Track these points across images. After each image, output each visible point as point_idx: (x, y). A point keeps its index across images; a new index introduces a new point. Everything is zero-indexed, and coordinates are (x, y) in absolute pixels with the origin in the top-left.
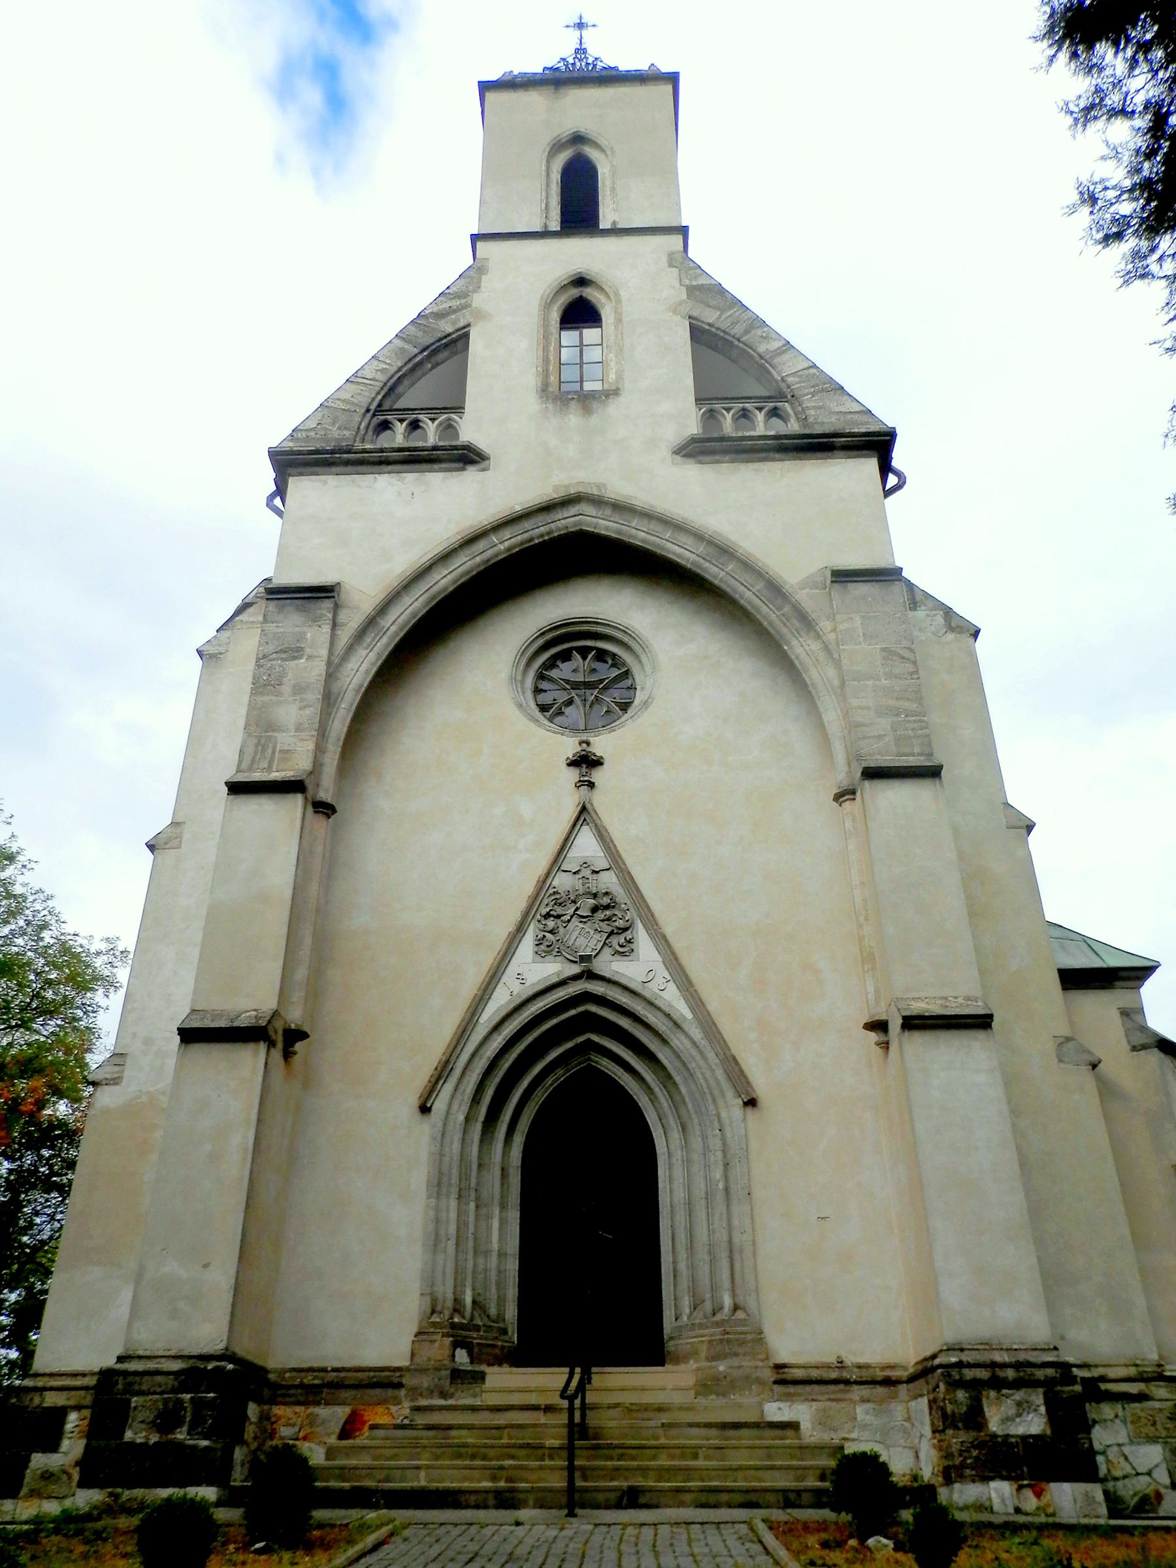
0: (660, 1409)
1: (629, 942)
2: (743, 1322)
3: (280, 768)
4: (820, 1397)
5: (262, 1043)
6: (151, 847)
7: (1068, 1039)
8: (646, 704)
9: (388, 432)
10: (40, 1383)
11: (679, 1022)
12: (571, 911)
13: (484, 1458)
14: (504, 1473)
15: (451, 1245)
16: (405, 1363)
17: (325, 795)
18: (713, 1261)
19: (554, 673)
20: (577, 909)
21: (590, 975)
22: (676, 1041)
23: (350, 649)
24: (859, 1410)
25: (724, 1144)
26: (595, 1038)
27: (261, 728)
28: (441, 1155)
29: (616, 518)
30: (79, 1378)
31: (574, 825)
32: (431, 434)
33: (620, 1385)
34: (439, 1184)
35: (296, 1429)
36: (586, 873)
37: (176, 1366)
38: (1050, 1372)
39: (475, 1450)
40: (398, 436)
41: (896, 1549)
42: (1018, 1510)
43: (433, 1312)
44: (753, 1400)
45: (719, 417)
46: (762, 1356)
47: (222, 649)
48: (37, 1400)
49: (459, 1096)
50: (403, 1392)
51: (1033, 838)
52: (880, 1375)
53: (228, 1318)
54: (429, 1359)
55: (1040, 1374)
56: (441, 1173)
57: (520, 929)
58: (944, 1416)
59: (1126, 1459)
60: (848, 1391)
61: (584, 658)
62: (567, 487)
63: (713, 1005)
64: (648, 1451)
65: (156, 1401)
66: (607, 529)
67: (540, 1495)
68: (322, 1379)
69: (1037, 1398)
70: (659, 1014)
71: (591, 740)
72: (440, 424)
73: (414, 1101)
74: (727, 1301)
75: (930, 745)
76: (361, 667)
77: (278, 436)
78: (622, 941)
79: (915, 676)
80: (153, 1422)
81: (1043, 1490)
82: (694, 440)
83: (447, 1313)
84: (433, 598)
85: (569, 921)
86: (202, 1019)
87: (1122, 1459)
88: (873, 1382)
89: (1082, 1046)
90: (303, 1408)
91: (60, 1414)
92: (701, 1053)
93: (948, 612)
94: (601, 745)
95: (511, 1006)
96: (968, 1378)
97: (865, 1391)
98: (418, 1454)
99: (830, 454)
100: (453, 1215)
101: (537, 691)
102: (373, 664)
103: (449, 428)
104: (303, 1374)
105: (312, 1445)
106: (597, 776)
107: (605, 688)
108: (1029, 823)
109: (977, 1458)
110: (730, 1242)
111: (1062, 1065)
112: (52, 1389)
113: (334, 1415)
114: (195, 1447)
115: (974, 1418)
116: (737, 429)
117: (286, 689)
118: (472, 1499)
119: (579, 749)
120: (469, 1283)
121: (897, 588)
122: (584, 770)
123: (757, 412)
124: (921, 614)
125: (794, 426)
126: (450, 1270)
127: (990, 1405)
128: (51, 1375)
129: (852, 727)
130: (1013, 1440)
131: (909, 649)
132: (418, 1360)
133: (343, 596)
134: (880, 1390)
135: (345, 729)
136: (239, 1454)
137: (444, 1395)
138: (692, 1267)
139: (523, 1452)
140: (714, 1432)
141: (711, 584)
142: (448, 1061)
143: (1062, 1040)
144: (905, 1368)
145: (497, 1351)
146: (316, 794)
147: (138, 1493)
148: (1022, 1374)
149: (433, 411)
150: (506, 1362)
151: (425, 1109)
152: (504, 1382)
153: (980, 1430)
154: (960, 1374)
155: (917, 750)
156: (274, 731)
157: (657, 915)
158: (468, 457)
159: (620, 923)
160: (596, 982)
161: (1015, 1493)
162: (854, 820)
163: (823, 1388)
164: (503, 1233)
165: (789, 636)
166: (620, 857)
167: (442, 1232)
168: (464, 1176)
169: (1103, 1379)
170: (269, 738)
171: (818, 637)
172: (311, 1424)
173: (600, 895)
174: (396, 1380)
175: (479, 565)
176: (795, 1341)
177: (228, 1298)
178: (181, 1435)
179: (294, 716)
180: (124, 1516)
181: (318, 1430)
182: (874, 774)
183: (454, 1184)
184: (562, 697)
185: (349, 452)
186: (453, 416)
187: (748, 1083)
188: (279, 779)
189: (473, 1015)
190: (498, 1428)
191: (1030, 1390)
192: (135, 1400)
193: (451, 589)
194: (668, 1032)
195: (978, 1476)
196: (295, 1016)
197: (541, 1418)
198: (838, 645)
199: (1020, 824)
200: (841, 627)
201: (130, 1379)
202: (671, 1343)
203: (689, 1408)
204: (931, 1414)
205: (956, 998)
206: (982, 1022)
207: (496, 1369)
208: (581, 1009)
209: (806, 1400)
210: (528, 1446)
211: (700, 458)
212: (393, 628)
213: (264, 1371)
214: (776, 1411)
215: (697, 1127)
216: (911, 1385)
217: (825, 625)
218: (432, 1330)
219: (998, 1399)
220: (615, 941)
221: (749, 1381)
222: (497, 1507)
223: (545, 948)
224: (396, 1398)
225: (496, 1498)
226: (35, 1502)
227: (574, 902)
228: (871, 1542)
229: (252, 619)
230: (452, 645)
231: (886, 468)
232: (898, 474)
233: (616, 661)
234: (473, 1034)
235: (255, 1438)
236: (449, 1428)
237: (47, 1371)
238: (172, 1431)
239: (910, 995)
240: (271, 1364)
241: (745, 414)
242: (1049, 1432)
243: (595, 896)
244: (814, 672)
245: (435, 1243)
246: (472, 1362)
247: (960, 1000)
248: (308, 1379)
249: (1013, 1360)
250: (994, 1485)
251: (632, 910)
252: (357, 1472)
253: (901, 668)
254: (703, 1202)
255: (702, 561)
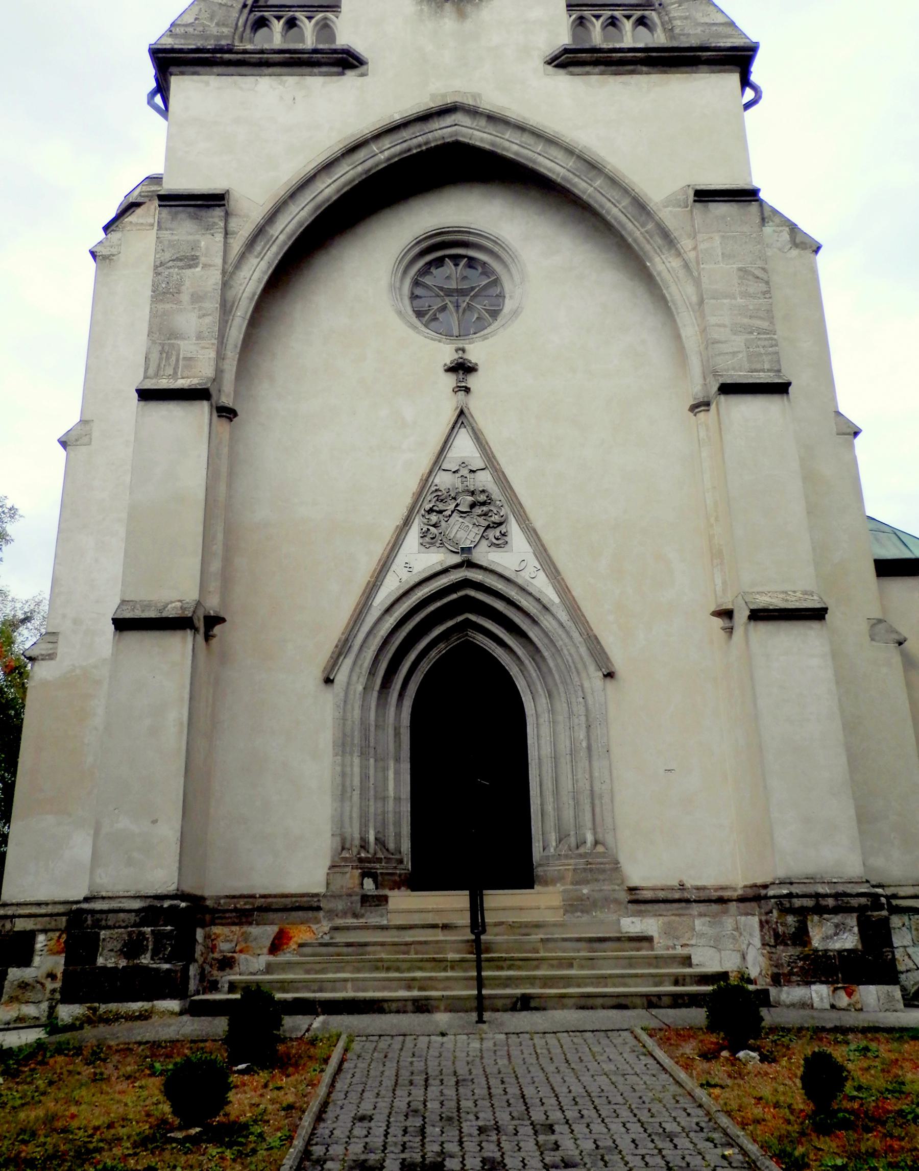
0: (538, 926)
1: (504, 535)
2: (603, 855)
3: (185, 375)
4: (665, 913)
5: (189, 631)
6: (64, 444)
7: (880, 621)
8: (516, 313)
9: (265, 29)
10: (10, 911)
11: (548, 606)
12: (452, 507)
13: (398, 970)
14: (416, 984)
15: (356, 796)
16: (321, 889)
17: (226, 400)
18: (577, 804)
19: (428, 280)
20: (457, 505)
21: (470, 564)
22: (545, 622)
23: (242, 257)
24: (697, 922)
25: (587, 710)
26: (473, 618)
27: (163, 337)
28: (344, 719)
29: (491, 129)
30: (43, 906)
31: (453, 428)
32: (309, 36)
33: (501, 903)
34: (343, 745)
35: (233, 944)
36: (464, 472)
37: (137, 905)
38: (863, 900)
39: (389, 964)
40: (275, 37)
41: (762, 1061)
42: (833, 1006)
43: (343, 849)
44: (614, 917)
45: (588, 24)
46: (619, 882)
47: (114, 251)
48: (8, 926)
49: (357, 669)
50: (321, 914)
51: (858, 441)
52: (715, 895)
53: (177, 865)
54: (342, 887)
55: (855, 902)
56: (344, 735)
57: (407, 523)
58: (776, 935)
59: (910, 957)
60: (688, 908)
61: (456, 265)
62: (444, 96)
63: (578, 592)
64: (531, 962)
65: (121, 934)
66: (482, 140)
67: (449, 1002)
68: (253, 904)
69: (852, 921)
70: (531, 599)
71: (467, 347)
72: (317, 23)
73: (316, 673)
74: (590, 838)
75: (778, 361)
76: (254, 274)
77: (154, 30)
78: (498, 534)
79: (767, 296)
80: (121, 950)
81: (854, 991)
82: (566, 51)
83: (355, 850)
84: (319, 207)
85: (450, 516)
86: (133, 610)
87: (906, 957)
88: (709, 901)
89: (891, 626)
90: (238, 928)
91: (30, 936)
92: (567, 633)
93: (793, 228)
94: (475, 352)
95: (401, 591)
96: (796, 906)
97: (702, 907)
98: (343, 967)
99: (694, 68)
100: (357, 770)
101: (413, 297)
102: (265, 273)
103: (325, 28)
104: (236, 900)
105: (247, 956)
106: (472, 381)
107: (475, 296)
108: (856, 430)
109: (802, 968)
110: (592, 791)
111: (874, 643)
112: (20, 916)
113: (265, 933)
114: (157, 970)
115: (801, 936)
116: (606, 39)
117: (185, 297)
118: (394, 1006)
119: (456, 356)
120: (371, 825)
121: (754, 207)
122: (461, 376)
123: (625, 20)
124: (768, 230)
125: (659, 39)
126: (356, 815)
127: (813, 926)
128: (18, 905)
129: (709, 343)
130: (832, 954)
131: (763, 269)
132: (332, 887)
133: (232, 203)
134: (715, 907)
135: (242, 336)
136: (193, 970)
137: (355, 916)
138: (558, 809)
139: (428, 965)
140: (583, 945)
141: (579, 198)
142: (347, 640)
143: (875, 621)
144: (735, 889)
145: (397, 878)
146: (219, 398)
147: (113, 1006)
148: (840, 902)
149: (311, 9)
150: (404, 885)
151: (328, 681)
152: (405, 903)
153: (805, 946)
154: (790, 902)
155: (767, 366)
156: (176, 338)
157: (528, 510)
158: (347, 61)
159: (496, 518)
160: (474, 570)
161: (831, 993)
162: (707, 430)
163: (668, 906)
164: (397, 782)
165: (652, 253)
166: (494, 457)
167: (348, 783)
168: (366, 737)
169: (895, 896)
170: (172, 345)
171: (679, 254)
172: (246, 940)
173: (477, 492)
174: (316, 904)
175: (361, 174)
176: (644, 869)
177: (175, 848)
178: (145, 960)
179: (194, 324)
180: (101, 1025)
181: (253, 944)
182: (728, 389)
183: (354, 743)
184: (437, 304)
185: (230, 51)
186: (329, 15)
187: (608, 658)
188: (186, 387)
189: (368, 598)
190: (407, 944)
191: (846, 915)
192: (103, 934)
193: (334, 198)
194: (538, 614)
195: (803, 981)
196: (213, 605)
197: (439, 936)
198: (698, 263)
199: (848, 431)
200: (702, 246)
201: (98, 916)
202: (540, 869)
203: (561, 925)
204: (761, 930)
205: (794, 592)
206: (817, 614)
207: (396, 892)
208: (461, 593)
209: (655, 915)
210: (434, 960)
211: (571, 69)
212: (282, 237)
213: (203, 898)
214: (632, 925)
215: (563, 695)
216: (741, 905)
217: (686, 243)
218: (343, 864)
219: (820, 922)
220: (491, 534)
221: (607, 901)
222: (414, 1012)
223: (430, 539)
224: (316, 918)
225: (414, 1004)
226: (15, 1006)
227: (455, 498)
228: (741, 1054)
229: (141, 221)
230: (334, 251)
231: (745, 82)
232: (755, 88)
233: (486, 270)
234: (369, 615)
235: (202, 954)
236: (366, 945)
237: (14, 901)
238: (137, 956)
239: (755, 590)
240: (206, 893)
241: (613, 22)
242: (860, 947)
243: (473, 493)
244: (673, 289)
245: (342, 794)
246: (377, 888)
247: (798, 594)
248: (241, 904)
249: (834, 891)
250: (814, 987)
251: (506, 506)
252: (295, 984)
253: (755, 287)
254: (568, 757)
255: (571, 176)
